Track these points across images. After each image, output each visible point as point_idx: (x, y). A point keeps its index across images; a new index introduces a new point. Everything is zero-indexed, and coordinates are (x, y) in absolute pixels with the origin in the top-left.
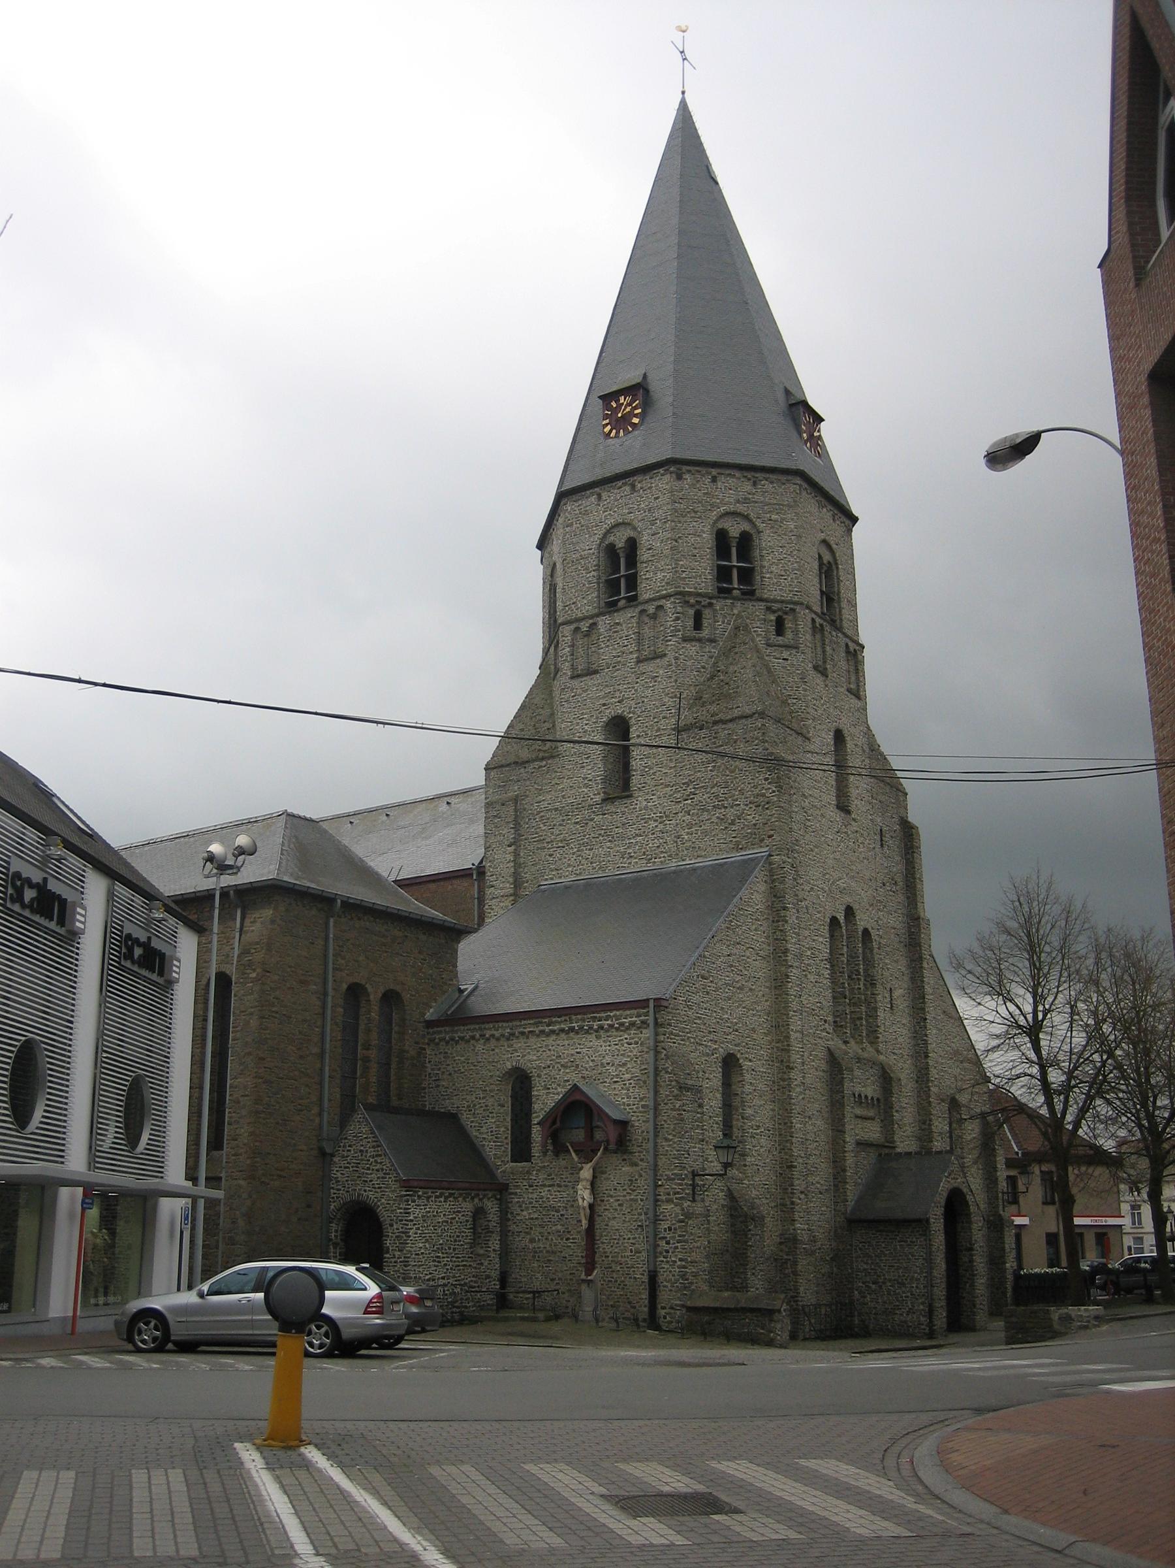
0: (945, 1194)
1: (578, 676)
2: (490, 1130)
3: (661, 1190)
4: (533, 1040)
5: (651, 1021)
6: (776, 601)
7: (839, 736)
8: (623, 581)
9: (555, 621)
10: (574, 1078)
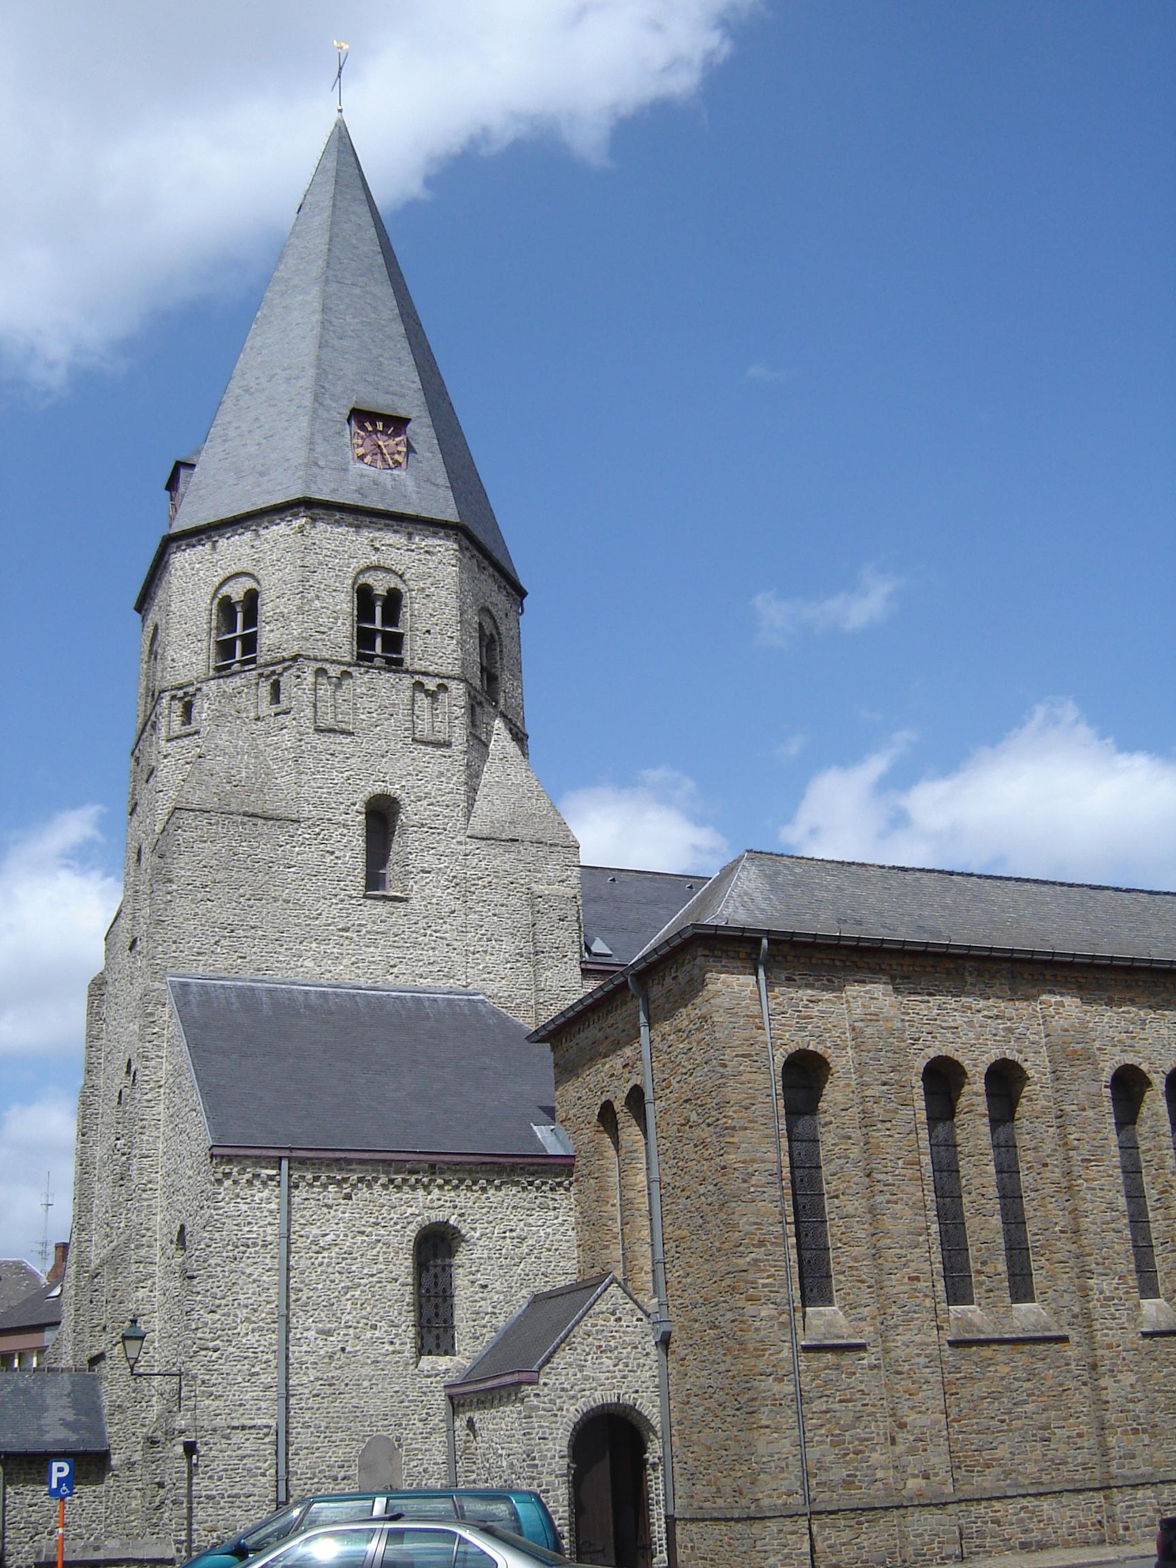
8: (239, 644)
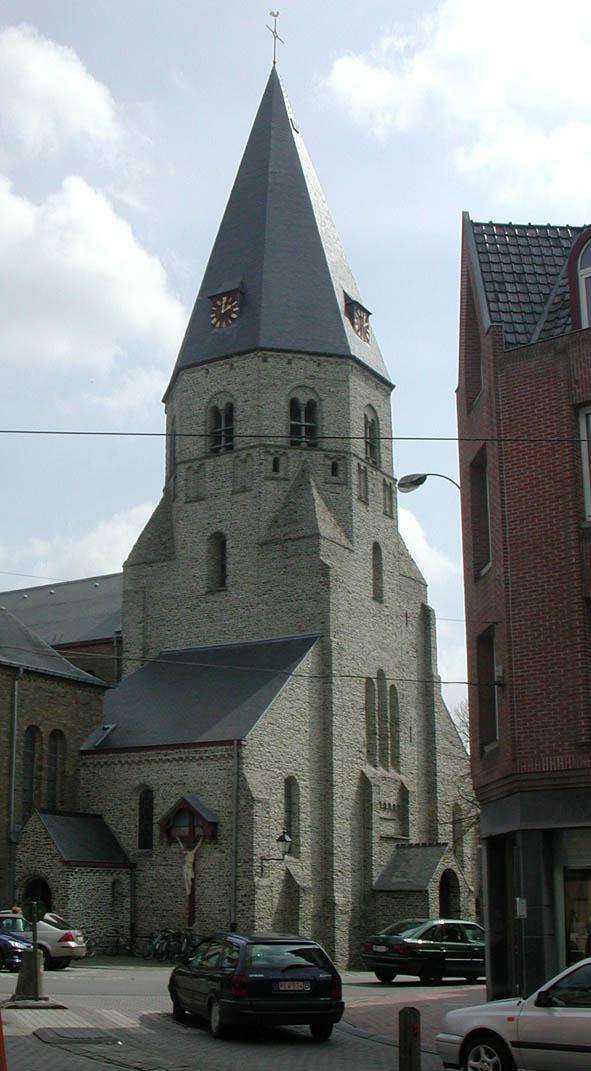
0: (441, 873)
1: (190, 502)
2: (125, 826)
3: (240, 869)
4: (154, 765)
5: (235, 755)
6: (331, 451)
7: (376, 547)
9: (174, 458)
10: (182, 792)
